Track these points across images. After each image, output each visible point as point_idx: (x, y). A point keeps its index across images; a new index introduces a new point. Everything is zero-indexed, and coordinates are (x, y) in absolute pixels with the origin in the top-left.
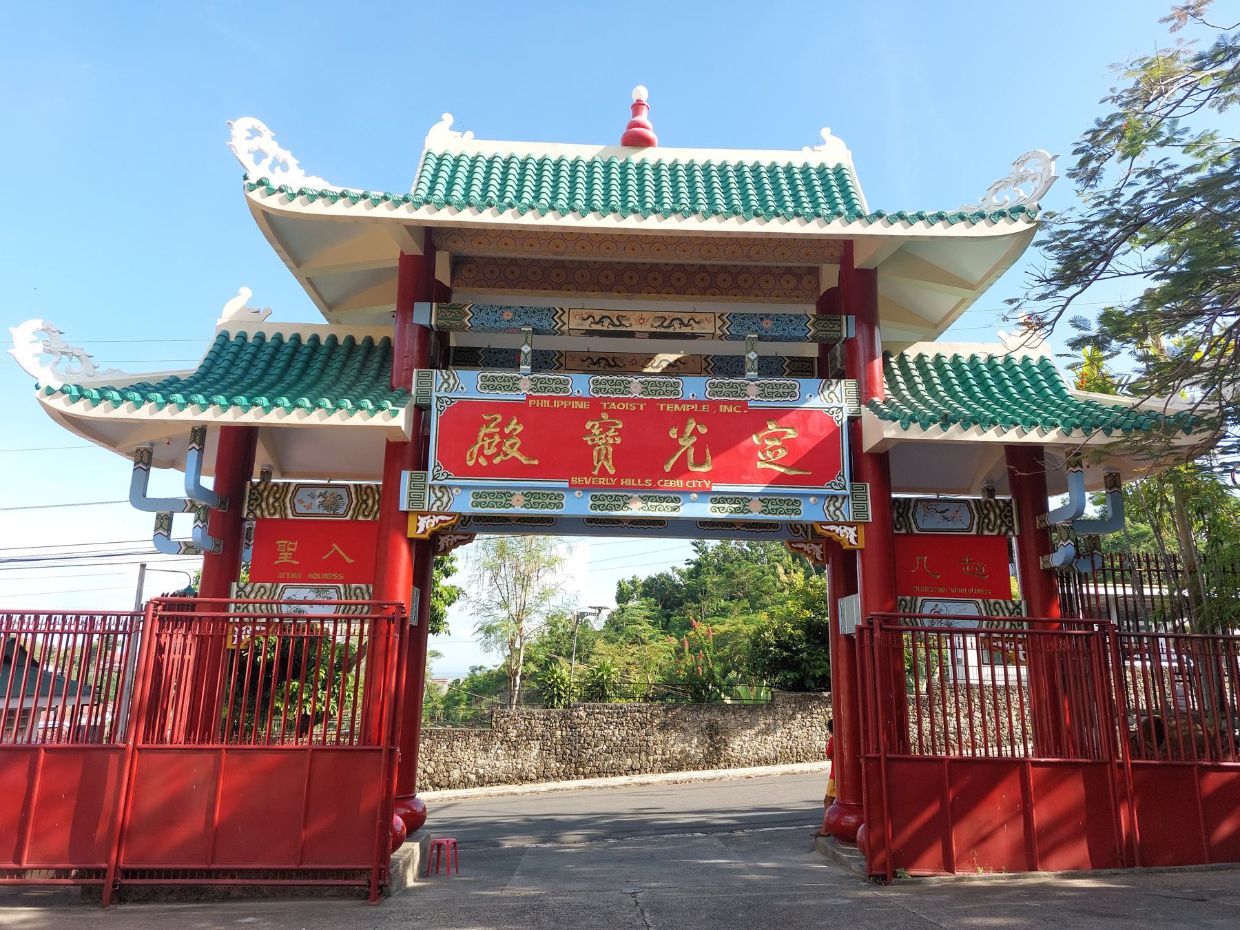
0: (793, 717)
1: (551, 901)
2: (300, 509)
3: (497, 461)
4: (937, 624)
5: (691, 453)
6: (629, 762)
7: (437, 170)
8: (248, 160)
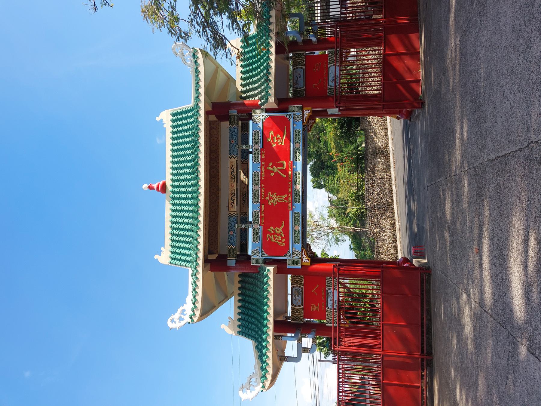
0: (369, 122)
1: (430, 214)
2: (300, 304)
3: (283, 235)
4: (338, 81)
5: (279, 168)
6: (387, 185)
7: (177, 259)
8: (183, 323)
